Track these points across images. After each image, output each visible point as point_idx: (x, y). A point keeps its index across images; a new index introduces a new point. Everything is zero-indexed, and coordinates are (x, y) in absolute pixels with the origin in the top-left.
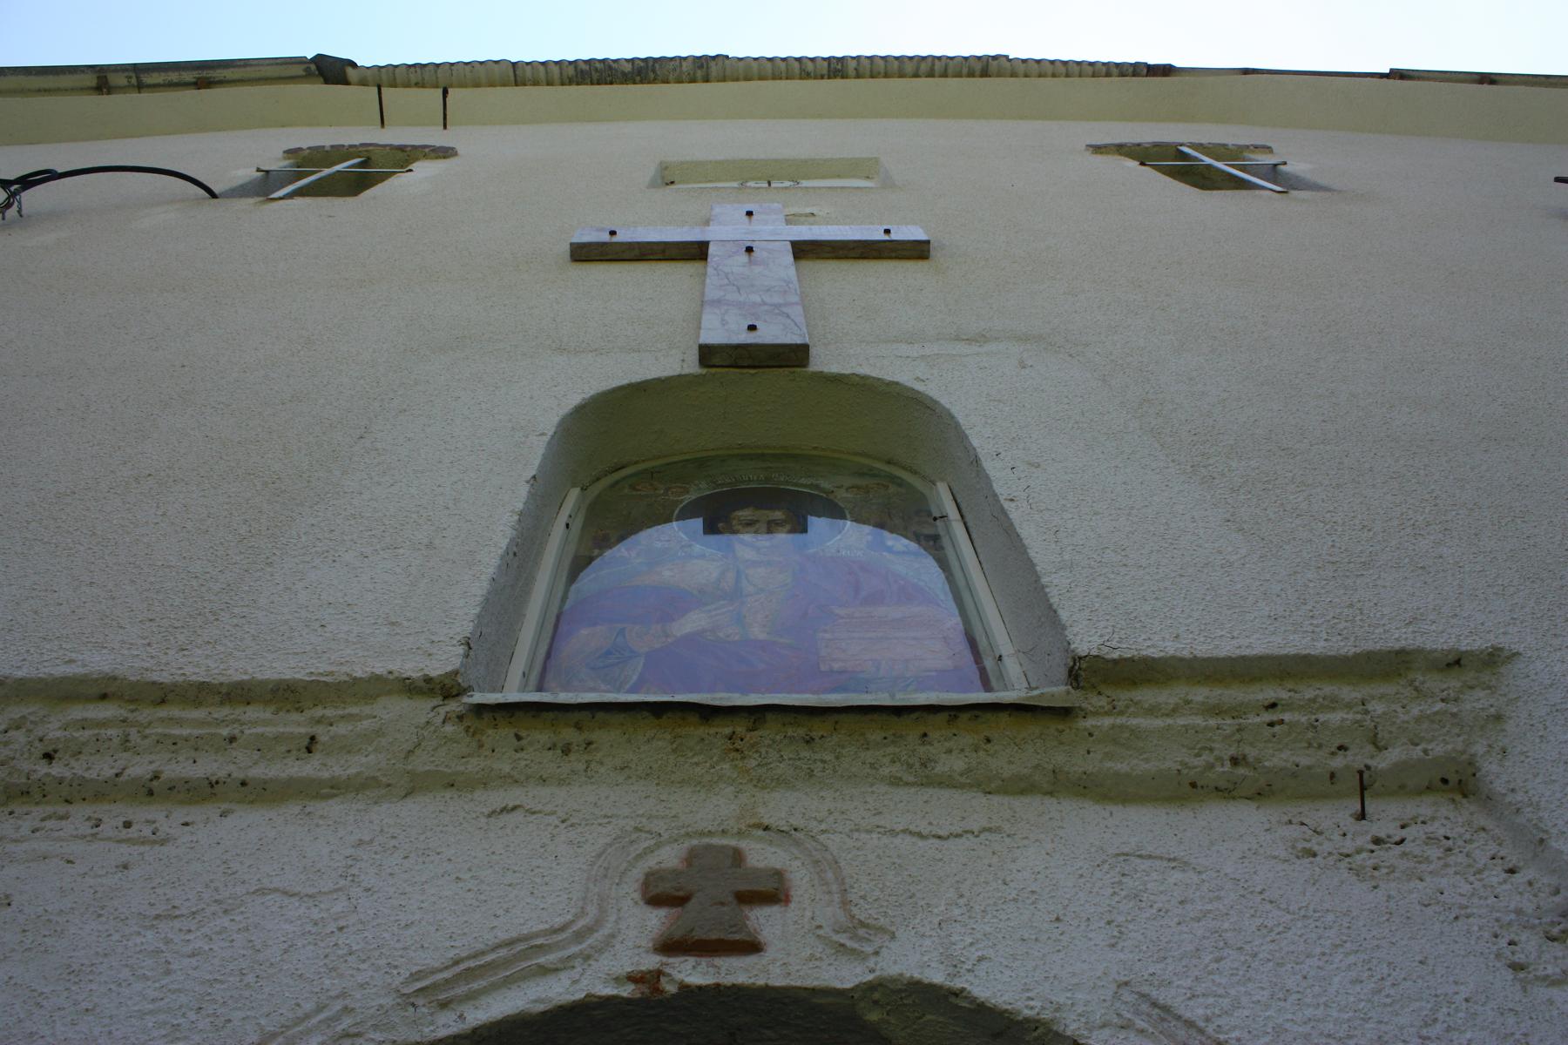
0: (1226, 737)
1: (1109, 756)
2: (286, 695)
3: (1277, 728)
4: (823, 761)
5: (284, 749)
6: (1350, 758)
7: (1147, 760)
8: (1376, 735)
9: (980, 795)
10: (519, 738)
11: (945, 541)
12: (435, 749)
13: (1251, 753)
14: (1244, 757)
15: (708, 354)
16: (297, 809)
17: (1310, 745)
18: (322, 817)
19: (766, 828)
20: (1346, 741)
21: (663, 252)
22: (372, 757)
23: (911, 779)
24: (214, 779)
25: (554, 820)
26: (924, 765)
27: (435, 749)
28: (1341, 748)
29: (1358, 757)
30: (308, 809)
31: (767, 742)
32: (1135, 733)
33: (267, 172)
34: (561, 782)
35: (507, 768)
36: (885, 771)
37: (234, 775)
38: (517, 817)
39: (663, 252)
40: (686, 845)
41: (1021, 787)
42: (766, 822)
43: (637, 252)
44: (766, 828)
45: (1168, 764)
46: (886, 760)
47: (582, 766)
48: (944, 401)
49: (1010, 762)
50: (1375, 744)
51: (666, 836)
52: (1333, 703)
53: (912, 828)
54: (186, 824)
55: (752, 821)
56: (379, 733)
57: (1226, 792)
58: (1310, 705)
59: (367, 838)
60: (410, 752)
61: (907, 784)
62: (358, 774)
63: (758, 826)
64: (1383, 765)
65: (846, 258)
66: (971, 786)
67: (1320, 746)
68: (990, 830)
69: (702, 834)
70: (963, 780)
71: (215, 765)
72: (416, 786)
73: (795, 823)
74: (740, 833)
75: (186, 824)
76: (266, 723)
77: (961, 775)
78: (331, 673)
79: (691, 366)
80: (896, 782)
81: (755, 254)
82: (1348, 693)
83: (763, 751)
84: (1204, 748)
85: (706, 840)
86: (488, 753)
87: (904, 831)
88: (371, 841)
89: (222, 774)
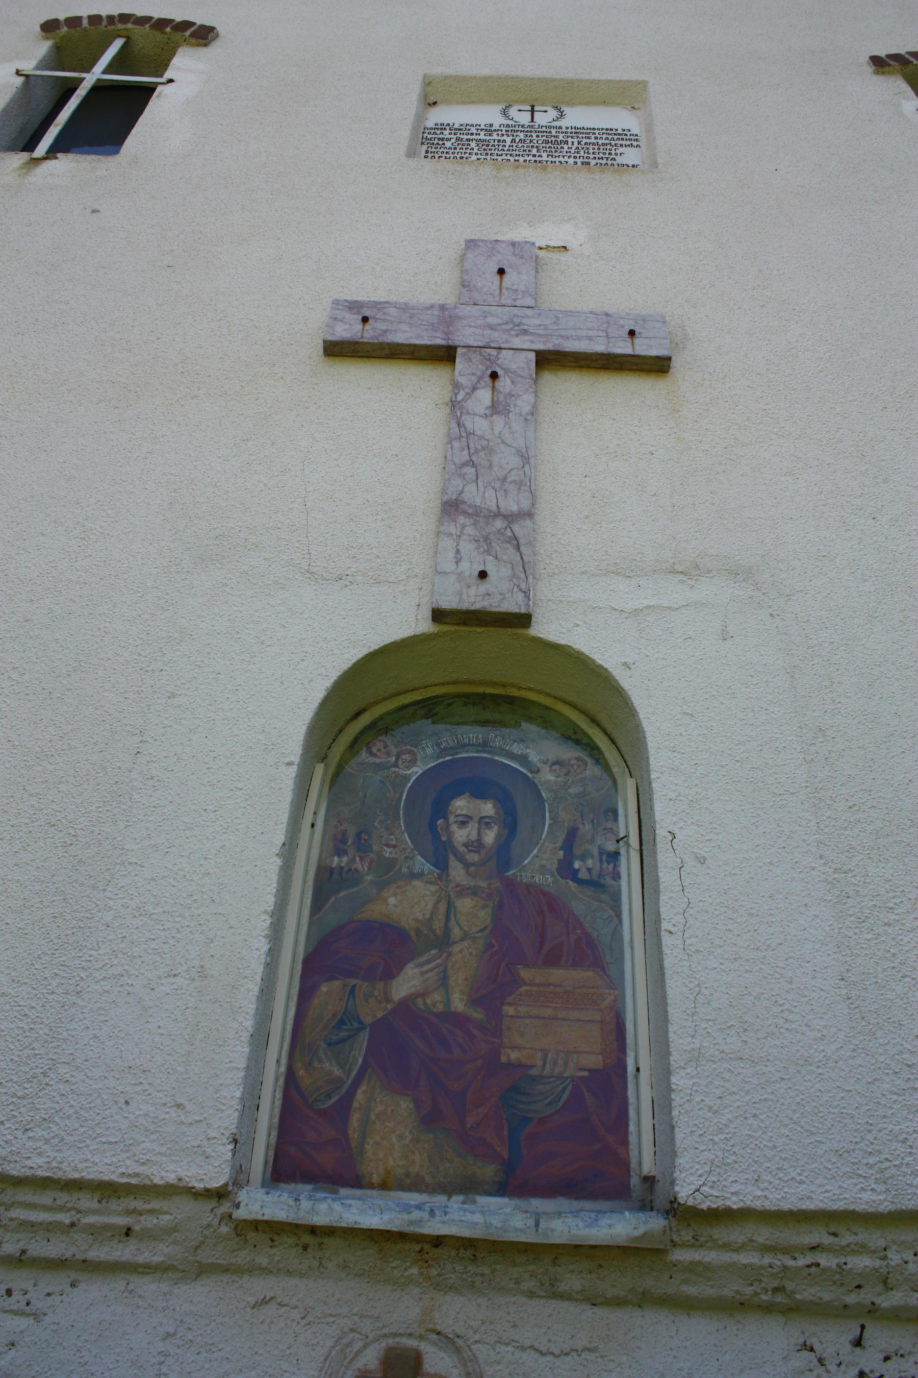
0: (773, 1274)
1: (686, 1282)
2: (107, 1190)
3: (813, 1269)
4: (483, 1275)
5: (109, 1234)
6: (862, 1296)
7: (712, 1287)
8: (887, 1278)
9: (588, 1307)
10: (272, 1240)
11: (623, 860)
12: (215, 1245)
13: (790, 1286)
14: (784, 1287)
15: (438, 615)
16: (123, 1284)
17: (835, 1283)
18: (140, 1296)
19: (439, 1333)
20: (862, 1283)
21: (413, 353)
22: (171, 1248)
23: (542, 1293)
24: (64, 1258)
25: (296, 1314)
26: (552, 1285)
27: (215, 1245)
28: (859, 1287)
29: (865, 1297)
30: (131, 1287)
31: (445, 1257)
32: (707, 1267)
33: (27, 76)
34: (302, 1275)
35: (265, 1264)
36: (525, 1286)
37: (77, 1256)
38: (271, 1308)
39: (413, 353)
40: (384, 1345)
41: (618, 1303)
42: (439, 1328)
43: (386, 351)
44: (439, 1333)
45: (726, 1292)
46: (526, 1276)
47: (316, 1264)
48: (643, 713)
49: (613, 1286)
50: (885, 1282)
51: (371, 1338)
52: (862, 1249)
53: (536, 1345)
54: (49, 1295)
55: (431, 1326)
56: (175, 1229)
57: (768, 1309)
58: (845, 1250)
59: (171, 1331)
60: (197, 1248)
61: (538, 1296)
62: (163, 1262)
63: (433, 1331)
64: (885, 1305)
65: (589, 367)
66: (583, 1300)
67: (842, 1284)
68: (589, 1350)
69: (396, 1335)
70: (578, 1296)
71: (63, 1245)
72: (202, 1270)
73: (458, 1331)
74: (421, 1337)
75: (49, 1295)
76: (95, 1212)
77: (577, 1293)
78: (137, 1175)
79: (425, 626)
80: (531, 1295)
81: (506, 278)
82: (876, 1239)
83: (442, 1263)
84: (756, 1280)
85: (397, 1339)
86: (252, 1248)
87: (532, 1347)
88: (175, 1334)
89: (68, 1255)
